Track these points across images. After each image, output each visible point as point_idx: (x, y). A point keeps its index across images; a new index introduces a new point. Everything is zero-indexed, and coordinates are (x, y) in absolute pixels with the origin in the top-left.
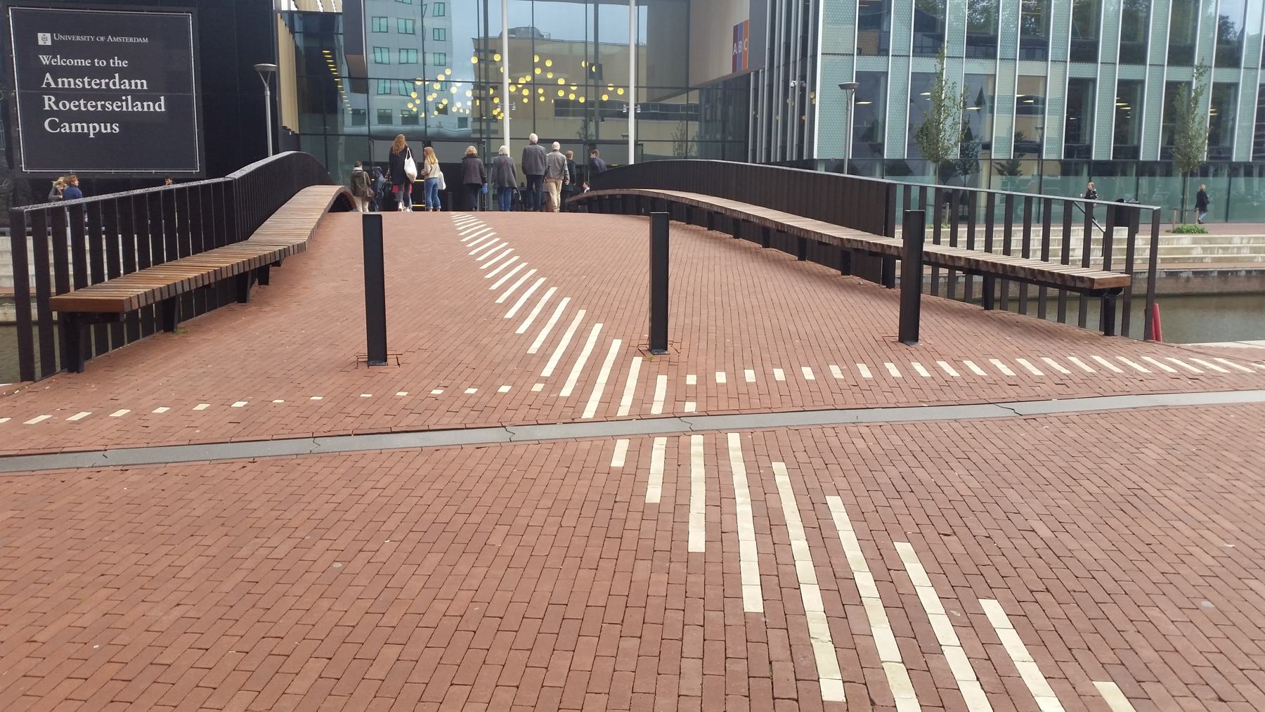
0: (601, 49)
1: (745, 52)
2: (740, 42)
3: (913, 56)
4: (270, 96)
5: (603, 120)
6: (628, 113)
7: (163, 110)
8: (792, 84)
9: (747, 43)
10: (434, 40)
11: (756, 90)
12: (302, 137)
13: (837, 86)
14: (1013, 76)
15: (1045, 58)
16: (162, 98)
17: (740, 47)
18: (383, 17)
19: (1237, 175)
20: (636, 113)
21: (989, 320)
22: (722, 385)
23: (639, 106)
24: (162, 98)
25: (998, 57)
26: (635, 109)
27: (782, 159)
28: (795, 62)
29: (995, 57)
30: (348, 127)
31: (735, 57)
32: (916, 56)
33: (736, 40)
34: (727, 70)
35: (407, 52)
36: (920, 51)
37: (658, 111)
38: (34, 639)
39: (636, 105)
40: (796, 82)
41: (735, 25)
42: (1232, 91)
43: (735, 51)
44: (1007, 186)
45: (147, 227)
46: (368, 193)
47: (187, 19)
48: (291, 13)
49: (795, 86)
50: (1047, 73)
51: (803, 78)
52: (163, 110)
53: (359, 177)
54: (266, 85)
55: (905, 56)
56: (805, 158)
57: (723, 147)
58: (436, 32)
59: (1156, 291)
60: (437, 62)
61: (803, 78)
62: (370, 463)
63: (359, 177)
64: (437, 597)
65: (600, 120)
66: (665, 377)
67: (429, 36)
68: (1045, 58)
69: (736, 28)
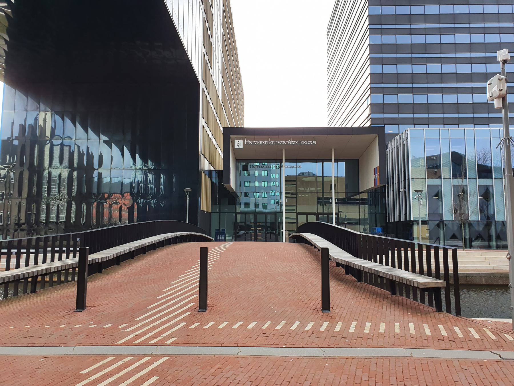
0: (325, 179)
1: (378, 178)
2: (376, 175)
3: (453, 178)
5: (326, 205)
6: (332, 202)
8: (401, 190)
11: (393, 191)
12: (212, 213)
13: (424, 190)
14: (450, 185)
15: (491, 177)
17: (376, 176)
19: (271, 223)
20: (335, 202)
21: (360, 288)
22: (397, 334)
23: (336, 200)
25: (493, 178)
27: (406, 220)
28: (402, 182)
29: (492, 178)
30: (243, 208)
31: (375, 180)
32: (454, 178)
33: (375, 174)
34: (372, 185)
36: (455, 176)
39: (335, 199)
40: (403, 189)
42: (343, 196)
43: (375, 178)
44: (366, 231)
45: (368, 258)
48: (210, 171)
49: (402, 191)
50: (493, 183)
51: (405, 188)
54: (188, 196)
55: (424, 178)
56: (408, 220)
57: (376, 215)
61: (405, 188)
62: (257, 378)
66: (380, 331)
68: (491, 177)
69: (374, 169)
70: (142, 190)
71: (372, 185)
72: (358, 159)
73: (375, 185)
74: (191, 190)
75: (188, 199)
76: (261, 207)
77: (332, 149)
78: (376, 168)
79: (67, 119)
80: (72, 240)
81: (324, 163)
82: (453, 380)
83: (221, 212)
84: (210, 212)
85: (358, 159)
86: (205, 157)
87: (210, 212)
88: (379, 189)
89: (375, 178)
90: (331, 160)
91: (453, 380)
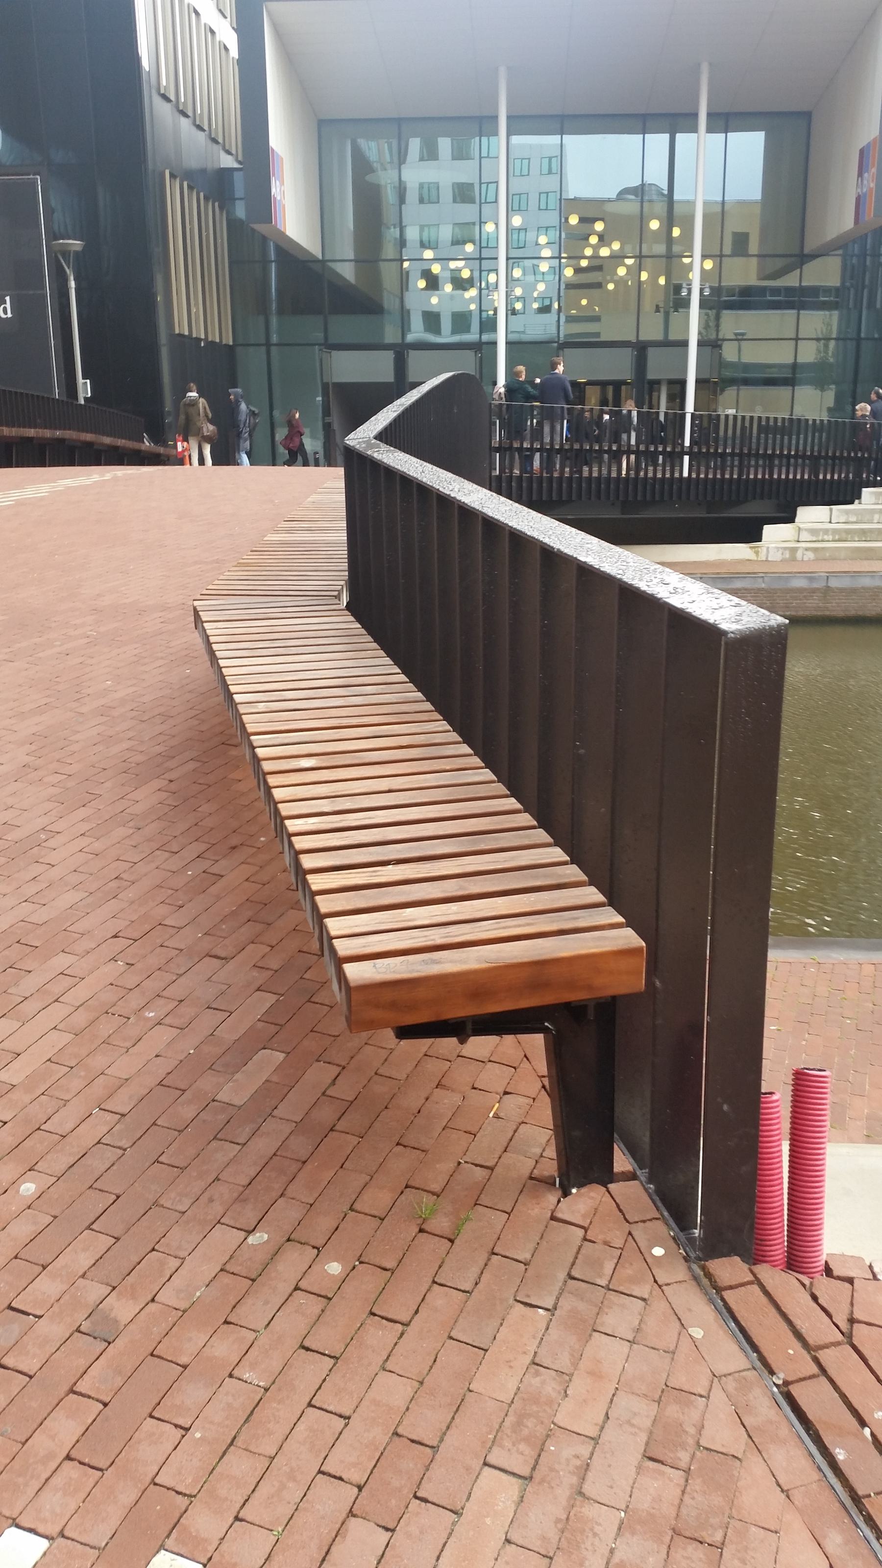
1: (871, 189)
4: (76, 289)
7: (9, 315)
9: (873, 173)
10: (540, 209)
12: (239, 350)
16: (8, 299)
17: (865, 182)
18: (491, 183)
24: (8, 299)
26: (702, 290)
31: (858, 199)
33: (860, 174)
35: (547, 230)
37: (832, 299)
38: (129, 966)
41: (860, 148)
43: (859, 190)
46: (205, 429)
47: (34, 183)
52: (9, 315)
53: (193, 405)
54: (68, 271)
58: (543, 196)
59: (536, 1042)
60: (522, 234)
63: (193, 405)
64: (36, 1168)
65: (672, 310)
67: (412, 196)
69: (862, 152)
70: (703, 462)
71: (848, 223)
72: (807, 116)
73: (857, 221)
74: (79, 249)
75: (73, 284)
76: (446, 324)
77: (699, 65)
78: (869, 145)
79: (348, 278)
80: (756, 537)
81: (679, 136)
82: (358, 1495)
83: (262, 345)
84: (231, 343)
85: (807, 116)
86: (227, 148)
87: (231, 343)
88: (869, 234)
89: (859, 190)
90: (695, 115)
91: (358, 1495)
